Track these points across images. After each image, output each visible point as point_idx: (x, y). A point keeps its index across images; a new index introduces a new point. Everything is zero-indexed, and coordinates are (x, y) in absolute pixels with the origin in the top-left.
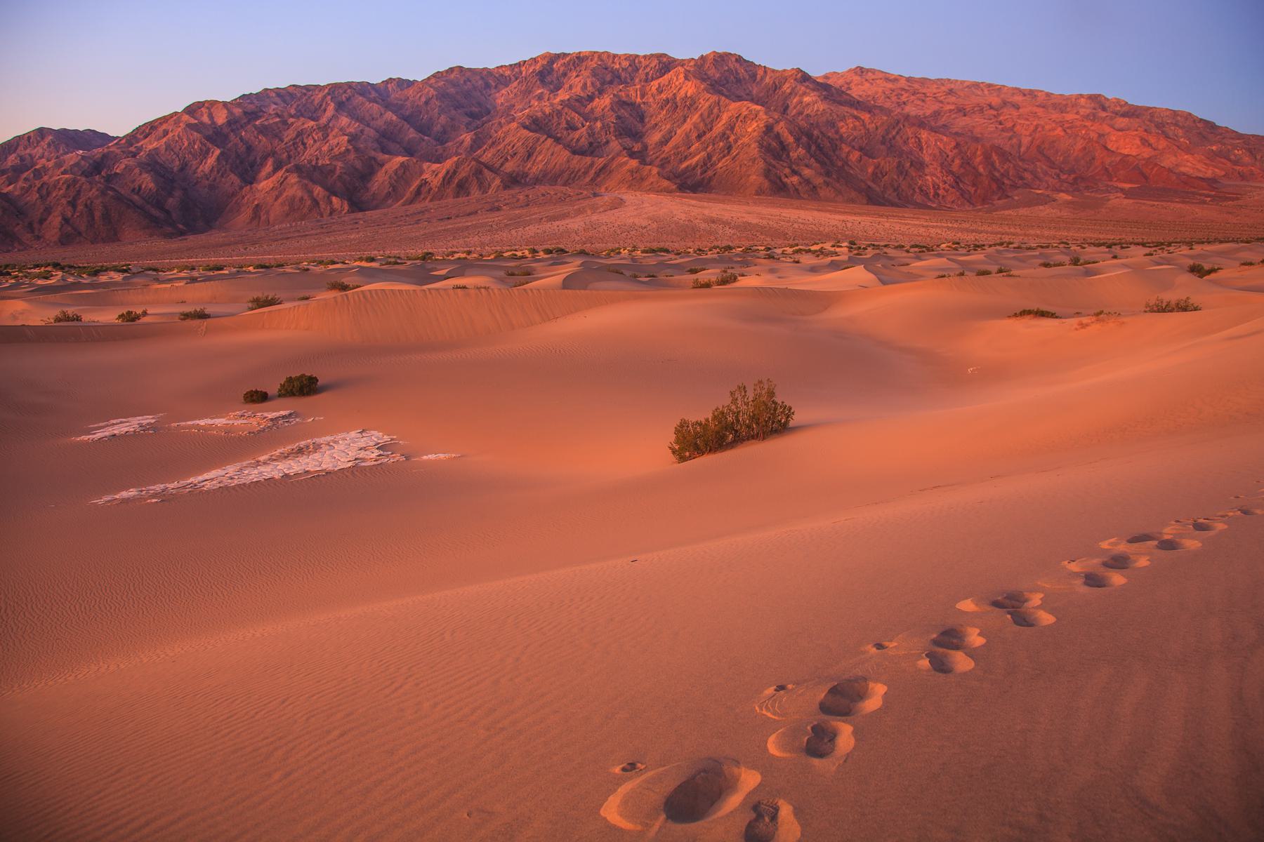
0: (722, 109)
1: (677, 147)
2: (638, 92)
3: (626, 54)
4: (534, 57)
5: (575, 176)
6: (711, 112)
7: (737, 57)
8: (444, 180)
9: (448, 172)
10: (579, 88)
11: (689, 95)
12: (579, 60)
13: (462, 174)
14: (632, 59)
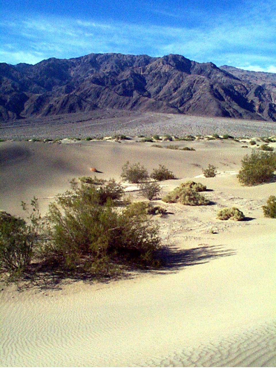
0: (184, 78)
1: (164, 94)
2: (141, 70)
3: (129, 55)
4: (87, 55)
5: (122, 105)
6: (179, 79)
7: (182, 57)
8: (62, 105)
9: (64, 102)
10: (110, 68)
11: (166, 71)
12: (107, 57)
13: (71, 101)
14: (132, 57)
